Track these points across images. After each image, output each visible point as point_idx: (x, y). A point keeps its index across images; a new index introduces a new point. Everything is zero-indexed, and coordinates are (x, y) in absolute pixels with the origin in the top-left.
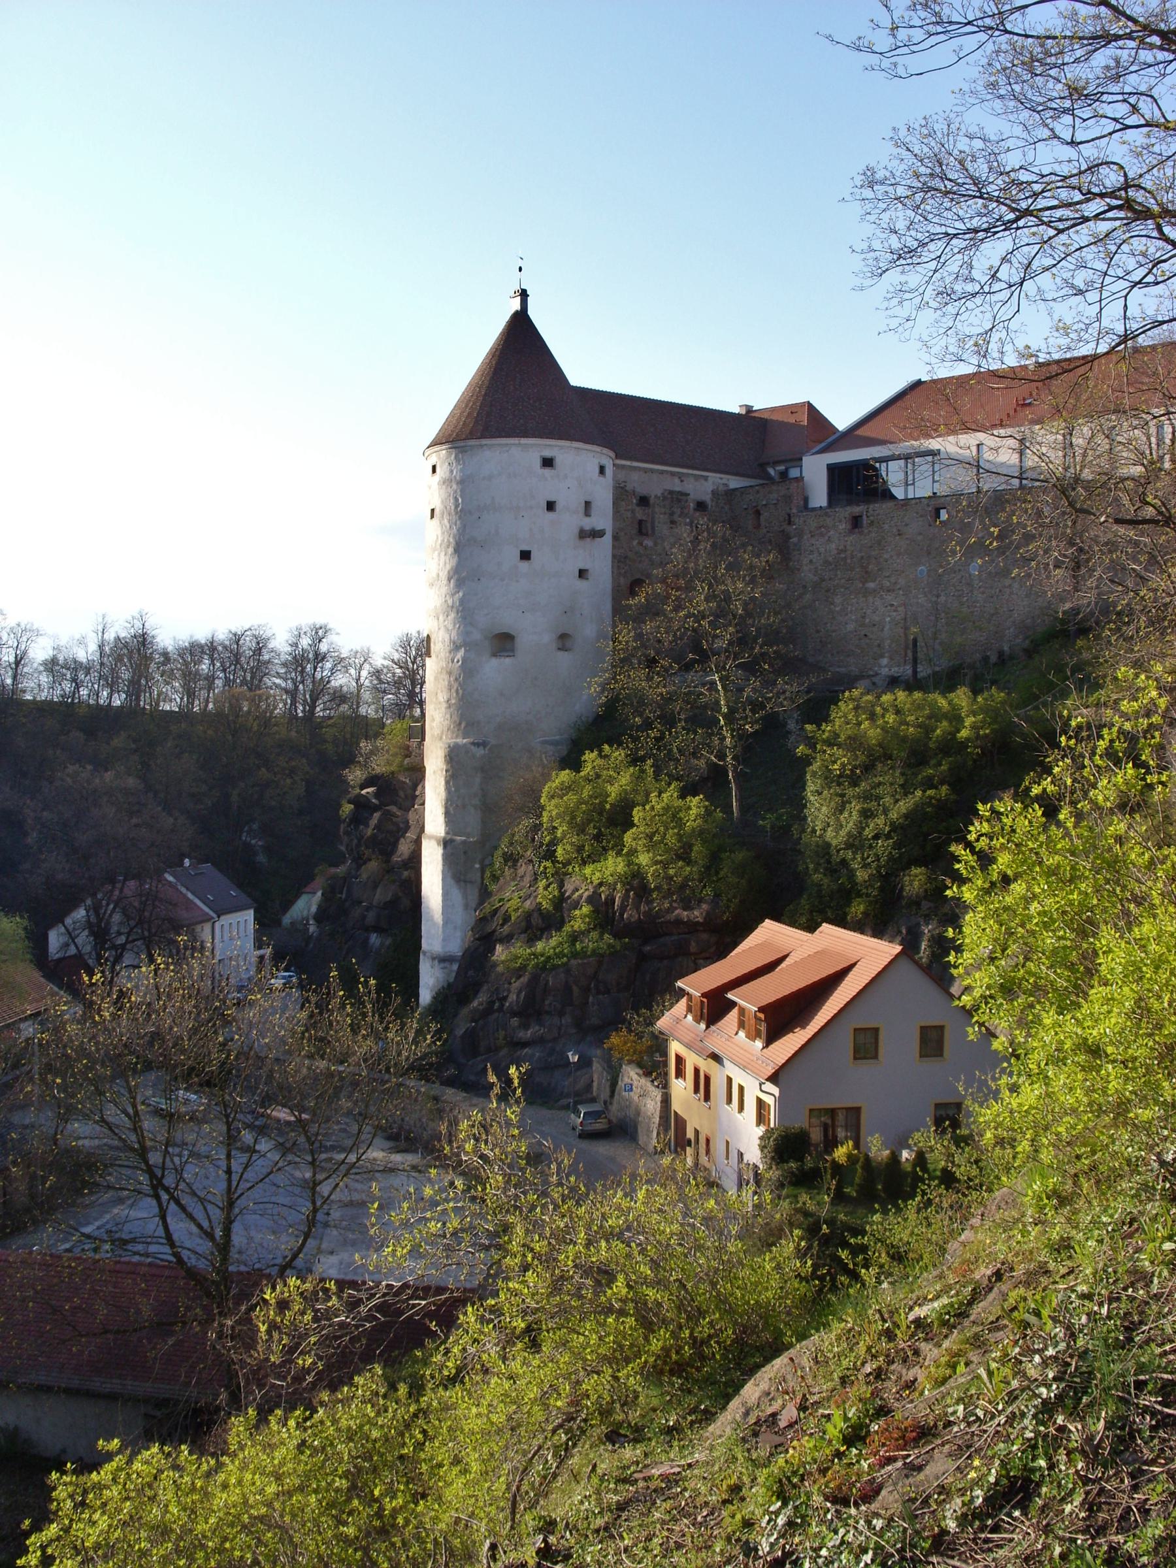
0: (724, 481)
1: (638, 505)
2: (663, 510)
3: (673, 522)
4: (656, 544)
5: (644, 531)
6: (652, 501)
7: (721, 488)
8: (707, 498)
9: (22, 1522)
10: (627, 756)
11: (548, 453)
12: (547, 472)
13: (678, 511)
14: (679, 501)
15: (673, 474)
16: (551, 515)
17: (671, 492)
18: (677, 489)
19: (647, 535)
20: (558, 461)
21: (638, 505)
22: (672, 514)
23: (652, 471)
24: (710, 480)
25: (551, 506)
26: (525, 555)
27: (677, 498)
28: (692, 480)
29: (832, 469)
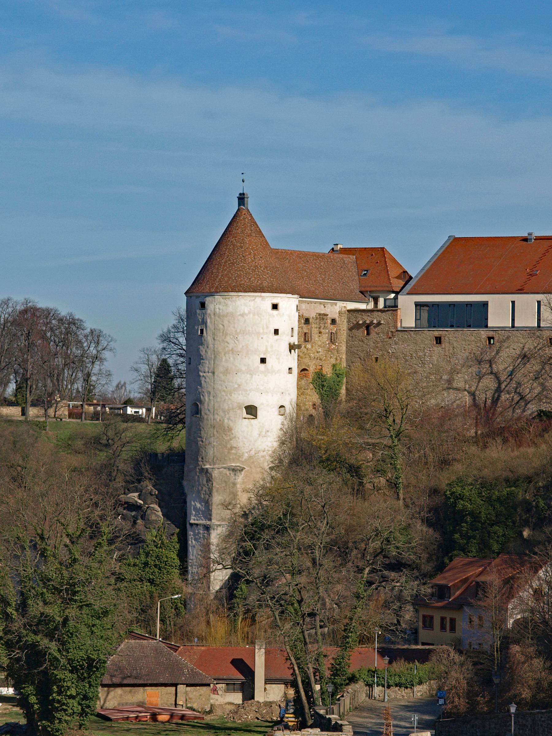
0: (344, 305)
1: (305, 324)
2: (316, 326)
3: (320, 333)
4: (312, 347)
5: (307, 339)
6: (311, 321)
7: (344, 309)
8: (336, 316)
9: (509, 710)
10: (106, 457)
11: (275, 301)
12: (275, 312)
13: (322, 326)
14: (323, 319)
15: (320, 303)
16: (276, 337)
17: (320, 314)
18: (322, 312)
19: (308, 341)
20: (280, 306)
21: (305, 324)
22: (320, 328)
23: (311, 302)
24: (338, 306)
25: (276, 332)
26: (263, 361)
27: (322, 317)
28: (329, 306)
29: (419, 305)
